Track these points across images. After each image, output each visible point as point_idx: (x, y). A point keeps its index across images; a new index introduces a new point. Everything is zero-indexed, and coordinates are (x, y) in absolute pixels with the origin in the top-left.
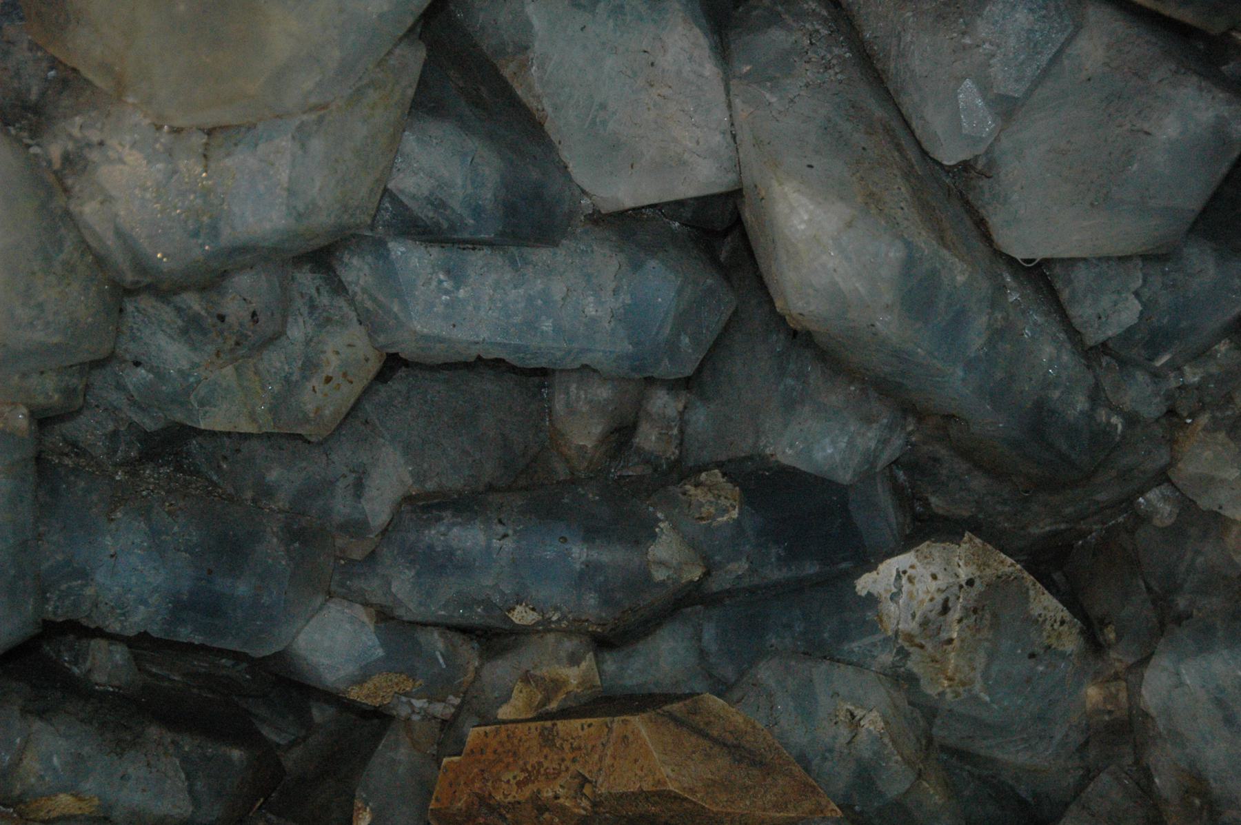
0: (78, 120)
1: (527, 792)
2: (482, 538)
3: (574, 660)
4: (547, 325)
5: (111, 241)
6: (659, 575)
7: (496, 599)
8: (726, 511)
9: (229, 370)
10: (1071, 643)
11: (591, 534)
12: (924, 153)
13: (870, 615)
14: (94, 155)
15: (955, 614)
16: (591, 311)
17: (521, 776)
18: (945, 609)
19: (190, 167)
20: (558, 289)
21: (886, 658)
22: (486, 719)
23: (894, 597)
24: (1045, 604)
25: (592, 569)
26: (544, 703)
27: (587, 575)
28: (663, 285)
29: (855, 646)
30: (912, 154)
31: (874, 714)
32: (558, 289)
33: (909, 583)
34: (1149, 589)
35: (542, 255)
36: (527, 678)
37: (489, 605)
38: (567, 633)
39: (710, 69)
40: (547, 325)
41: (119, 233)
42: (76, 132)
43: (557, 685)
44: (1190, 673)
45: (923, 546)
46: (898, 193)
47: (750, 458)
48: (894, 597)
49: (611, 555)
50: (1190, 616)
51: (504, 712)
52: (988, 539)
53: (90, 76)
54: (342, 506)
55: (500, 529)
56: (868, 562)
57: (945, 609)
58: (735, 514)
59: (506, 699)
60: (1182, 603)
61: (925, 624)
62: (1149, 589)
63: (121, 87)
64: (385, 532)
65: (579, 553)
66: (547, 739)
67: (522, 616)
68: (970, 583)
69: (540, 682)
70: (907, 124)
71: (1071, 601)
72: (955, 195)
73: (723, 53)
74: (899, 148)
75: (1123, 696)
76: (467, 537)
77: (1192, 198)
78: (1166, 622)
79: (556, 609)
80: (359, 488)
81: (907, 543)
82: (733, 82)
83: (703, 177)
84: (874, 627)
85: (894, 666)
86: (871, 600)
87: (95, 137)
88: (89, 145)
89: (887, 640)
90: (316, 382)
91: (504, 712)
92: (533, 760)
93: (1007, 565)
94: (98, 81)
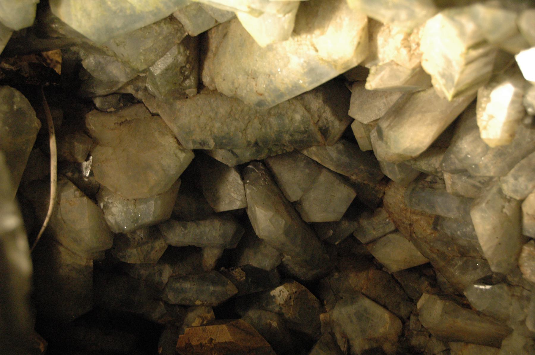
0: (107, 198)
1: (199, 342)
2: (189, 286)
3: (209, 312)
4: (205, 238)
5: (114, 223)
6: (229, 293)
7: (192, 299)
8: (242, 277)
9: (135, 250)
10: (317, 305)
11: (214, 283)
12: (286, 199)
13: (274, 300)
14: (111, 205)
15: (292, 300)
16: (214, 234)
17: (198, 339)
18: (290, 298)
19: (131, 207)
20: (207, 230)
21: (277, 309)
22: (188, 326)
23: (279, 296)
24: (312, 296)
25: (214, 291)
26: (203, 322)
27: (212, 294)
28: (230, 228)
29: (270, 307)
30: (284, 199)
31: (275, 322)
32: (207, 230)
33: (281, 293)
34: (333, 292)
35: (202, 222)
36: (199, 316)
37: (190, 300)
38: (207, 306)
39: (240, 181)
40: (205, 238)
41: (116, 222)
42: (106, 200)
43: (206, 318)
44: (343, 310)
45: (285, 284)
46: (282, 209)
47: (247, 265)
48: (279, 296)
49: (219, 289)
50: (342, 298)
51: (193, 325)
52: (299, 282)
53: (109, 188)
54: (157, 278)
55: (193, 283)
56: (273, 287)
57: (290, 298)
58: (244, 278)
59: (194, 322)
60: (341, 295)
61: (286, 301)
62: (333, 292)
63: (116, 191)
64: (166, 284)
65: (212, 288)
66: (204, 330)
67: (198, 303)
68: (296, 292)
69: (201, 317)
70: (283, 193)
71: (318, 297)
72: (294, 208)
73: (243, 179)
74: (281, 198)
75: (328, 316)
76: (187, 285)
77: (343, 209)
78: (338, 298)
79: (206, 301)
80: (161, 275)
81: (281, 284)
82: (246, 185)
83: (237, 205)
84: (275, 302)
85: (279, 311)
86: (274, 297)
87: (110, 201)
88: (109, 203)
89: (277, 306)
90: (154, 252)
91: (193, 325)
92: (201, 335)
93: (304, 288)
94: (111, 189)
